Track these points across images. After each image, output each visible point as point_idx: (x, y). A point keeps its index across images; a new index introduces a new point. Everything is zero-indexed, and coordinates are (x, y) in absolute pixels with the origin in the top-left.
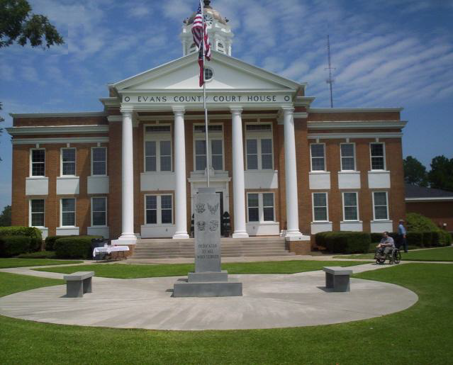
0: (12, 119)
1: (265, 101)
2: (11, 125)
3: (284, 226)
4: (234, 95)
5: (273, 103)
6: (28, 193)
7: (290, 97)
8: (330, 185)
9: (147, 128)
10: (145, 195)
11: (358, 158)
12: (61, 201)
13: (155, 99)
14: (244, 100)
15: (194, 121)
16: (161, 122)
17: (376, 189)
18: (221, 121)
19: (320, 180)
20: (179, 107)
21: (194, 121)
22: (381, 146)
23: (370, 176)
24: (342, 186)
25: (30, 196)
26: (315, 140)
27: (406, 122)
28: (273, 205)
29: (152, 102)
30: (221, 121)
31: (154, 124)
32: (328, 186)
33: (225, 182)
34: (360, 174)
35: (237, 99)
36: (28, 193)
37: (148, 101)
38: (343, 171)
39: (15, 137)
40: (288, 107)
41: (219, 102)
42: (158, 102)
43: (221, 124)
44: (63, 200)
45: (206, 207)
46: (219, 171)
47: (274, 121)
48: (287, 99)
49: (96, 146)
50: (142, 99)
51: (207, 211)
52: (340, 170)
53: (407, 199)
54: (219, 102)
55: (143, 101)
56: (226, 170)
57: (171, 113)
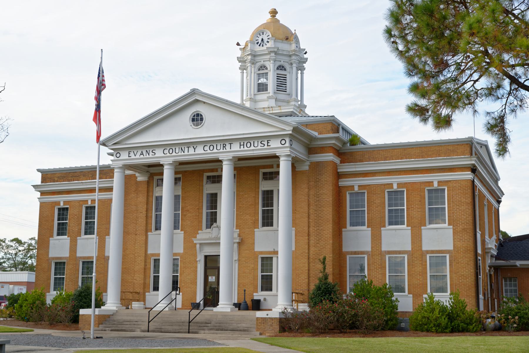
0: (40, 175)
1: (259, 147)
2: (39, 182)
4: (225, 142)
5: (253, 150)
6: (51, 255)
7: (288, 140)
9: (208, 177)
10: (428, 256)
11: (407, 208)
12: (81, 264)
13: (144, 153)
14: (236, 147)
17: (84, 258)
18: (210, 170)
19: (87, 246)
20: (226, 155)
25: (53, 258)
26: (352, 187)
28: (55, 278)
29: (142, 156)
35: (228, 146)
36: (51, 255)
37: (138, 156)
39: (43, 193)
41: (209, 151)
42: (148, 156)
44: (56, 263)
48: (283, 142)
49: (392, 188)
50: (132, 154)
54: (209, 151)
55: (133, 156)
57: (276, 157)
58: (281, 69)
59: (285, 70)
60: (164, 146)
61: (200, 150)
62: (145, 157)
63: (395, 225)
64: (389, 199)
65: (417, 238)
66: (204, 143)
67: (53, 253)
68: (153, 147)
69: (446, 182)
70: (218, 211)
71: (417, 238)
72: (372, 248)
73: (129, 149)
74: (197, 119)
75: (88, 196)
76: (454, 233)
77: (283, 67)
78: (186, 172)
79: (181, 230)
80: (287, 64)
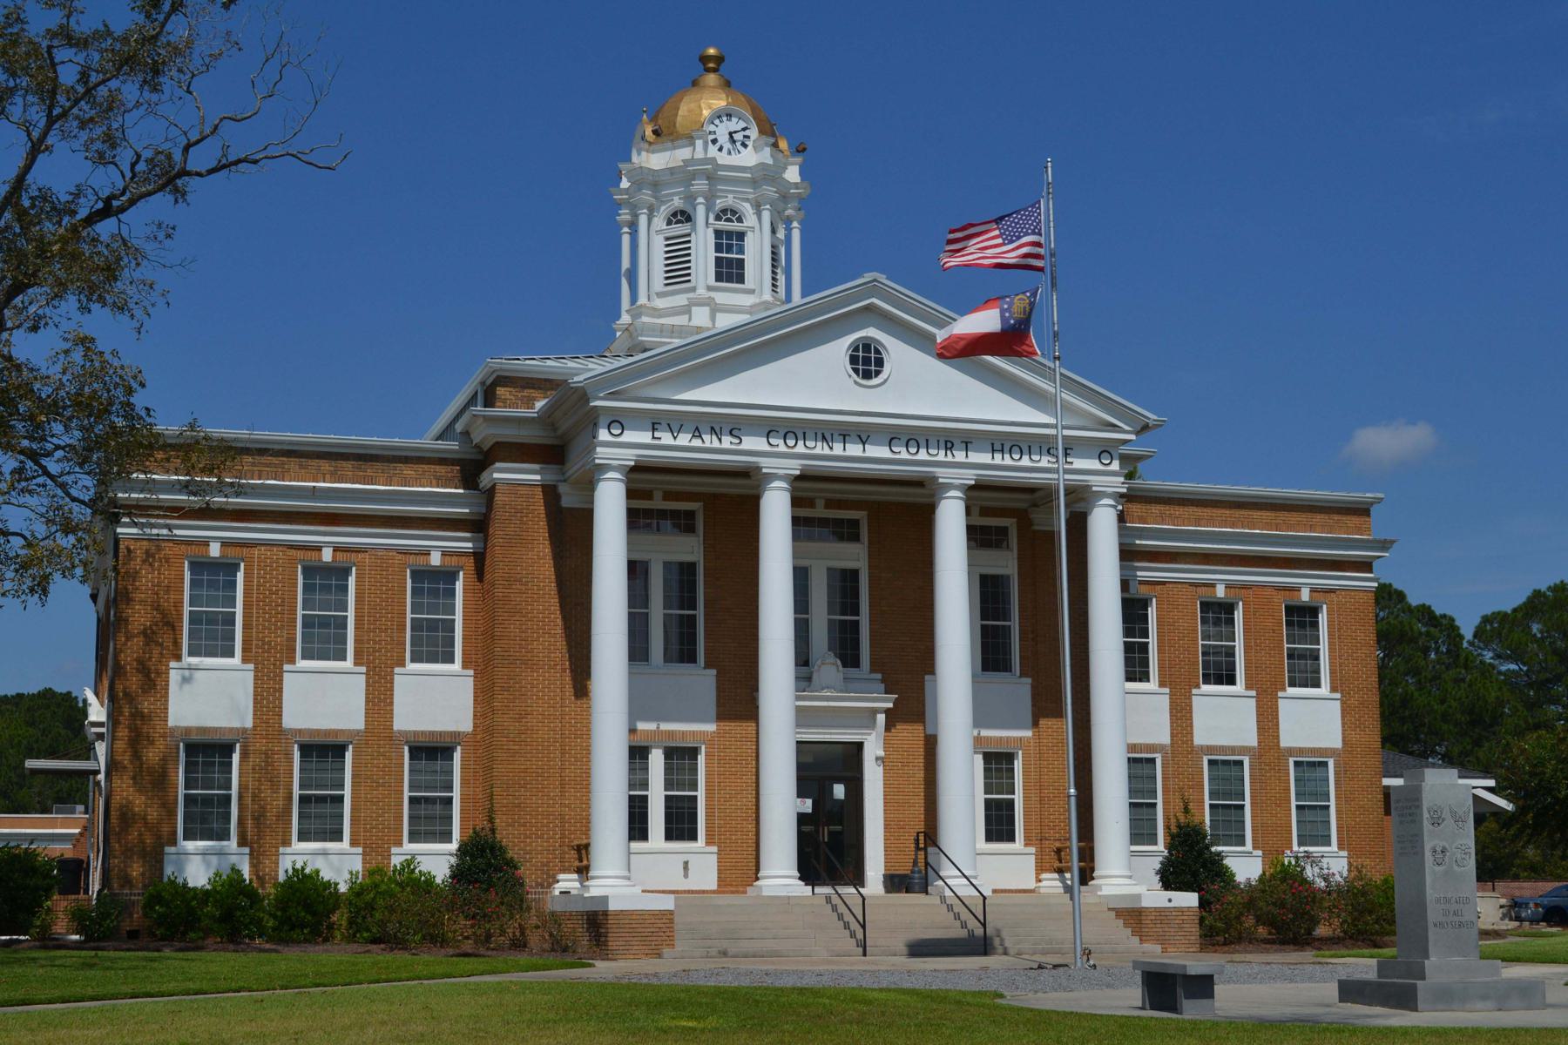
3: (742, 867)
4: (950, 439)
8: (363, 719)
10: (1291, 761)
15: (826, 505)
16: (831, 504)
18: (900, 515)
20: (780, 461)
21: (826, 505)
22: (1314, 611)
23: (1283, 705)
24: (1204, 734)
26: (1296, 589)
27: (1392, 542)
30: (900, 515)
31: (700, 513)
32: (1251, 740)
33: (875, 711)
34: (1257, 697)
38: (302, 664)
40: (1106, 478)
43: (1009, 522)
45: (1446, 814)
46: (852, 672)
47: (1023, 517)
51: (1449, 822)
52: (292, 661)
53: (31, 764)
56: (872, 671)
58: (728, 220)
59: (740, 220)
60: (771, 428)
61: (875, 451)
62: (707, 444)
63: (428, 661)
64: (307, 588)
65: (1268, 720)
66: (893, 436)
67: (1204, 734)
68: (734, 425)
69: (1245, 586)
70: (979, 623)
71: (1268, 720)
72: (1172, 735)
73: (655, 423)
74: (867, 362)
75: (325, 534)
76: (1343, 710)
77: (734, 212)
78: (715, 496)
79: (708, 666)
80: (747, 205)
